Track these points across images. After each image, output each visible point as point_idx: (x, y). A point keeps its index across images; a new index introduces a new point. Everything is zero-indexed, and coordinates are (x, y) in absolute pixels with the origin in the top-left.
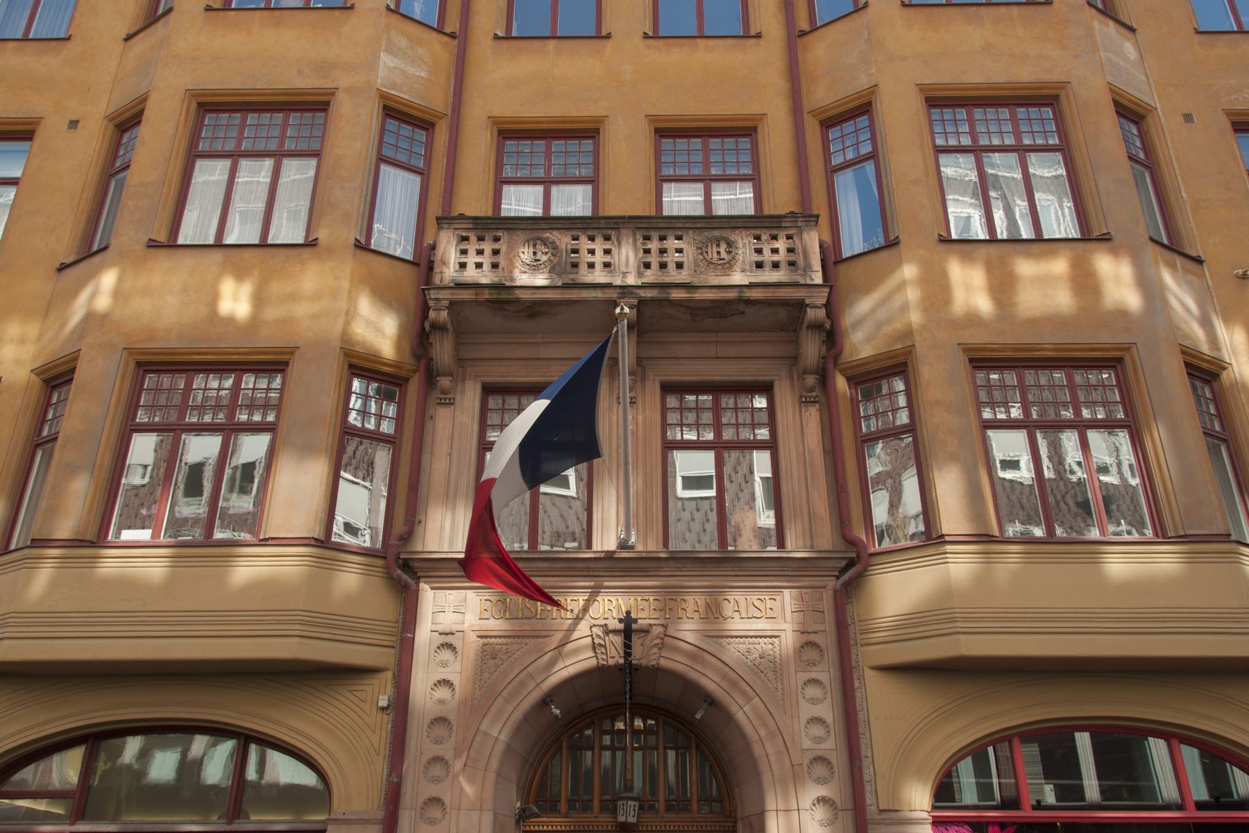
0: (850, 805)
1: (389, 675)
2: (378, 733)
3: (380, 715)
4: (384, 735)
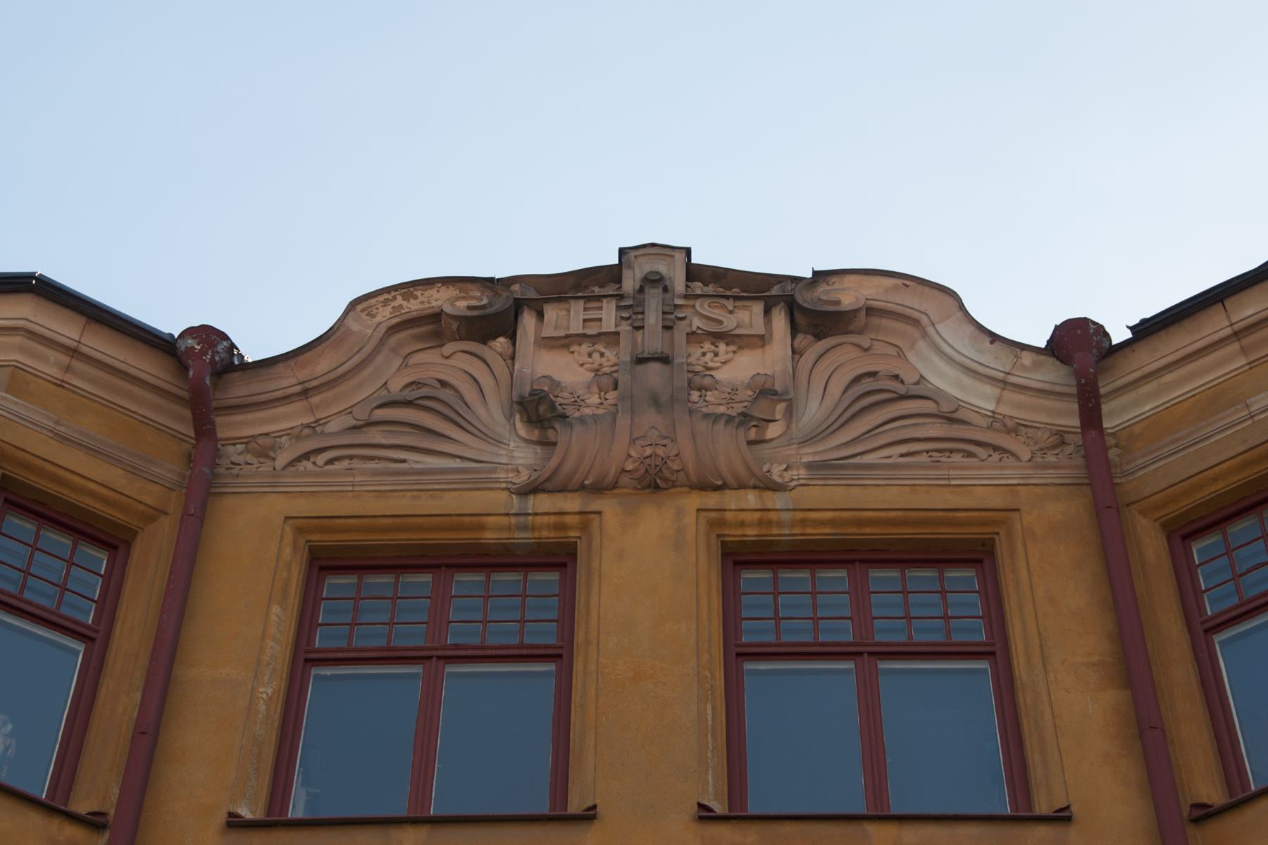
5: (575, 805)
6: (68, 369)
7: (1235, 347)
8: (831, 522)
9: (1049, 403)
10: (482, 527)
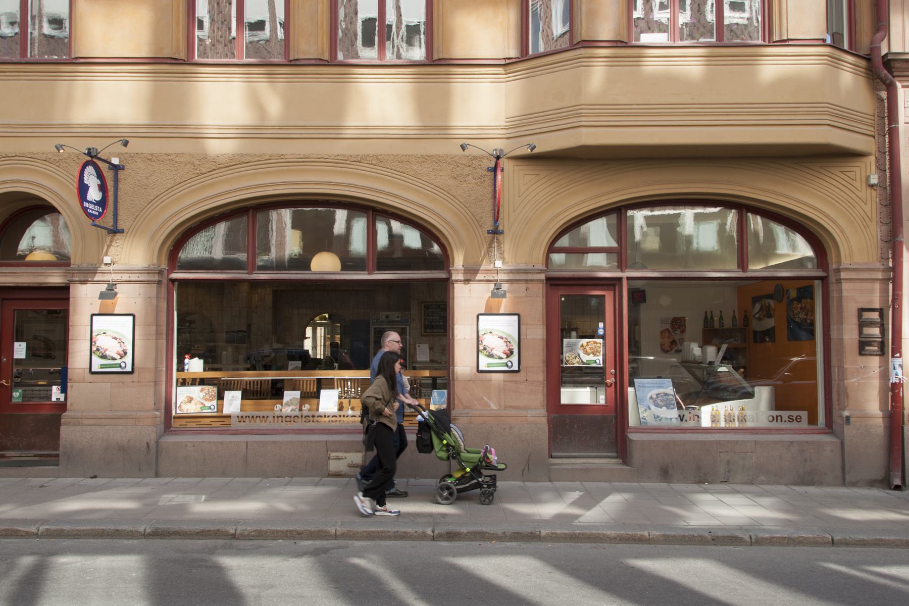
1: (872, 159)
2: (870, 205)
3: (869, 190)
4: (874, 206)
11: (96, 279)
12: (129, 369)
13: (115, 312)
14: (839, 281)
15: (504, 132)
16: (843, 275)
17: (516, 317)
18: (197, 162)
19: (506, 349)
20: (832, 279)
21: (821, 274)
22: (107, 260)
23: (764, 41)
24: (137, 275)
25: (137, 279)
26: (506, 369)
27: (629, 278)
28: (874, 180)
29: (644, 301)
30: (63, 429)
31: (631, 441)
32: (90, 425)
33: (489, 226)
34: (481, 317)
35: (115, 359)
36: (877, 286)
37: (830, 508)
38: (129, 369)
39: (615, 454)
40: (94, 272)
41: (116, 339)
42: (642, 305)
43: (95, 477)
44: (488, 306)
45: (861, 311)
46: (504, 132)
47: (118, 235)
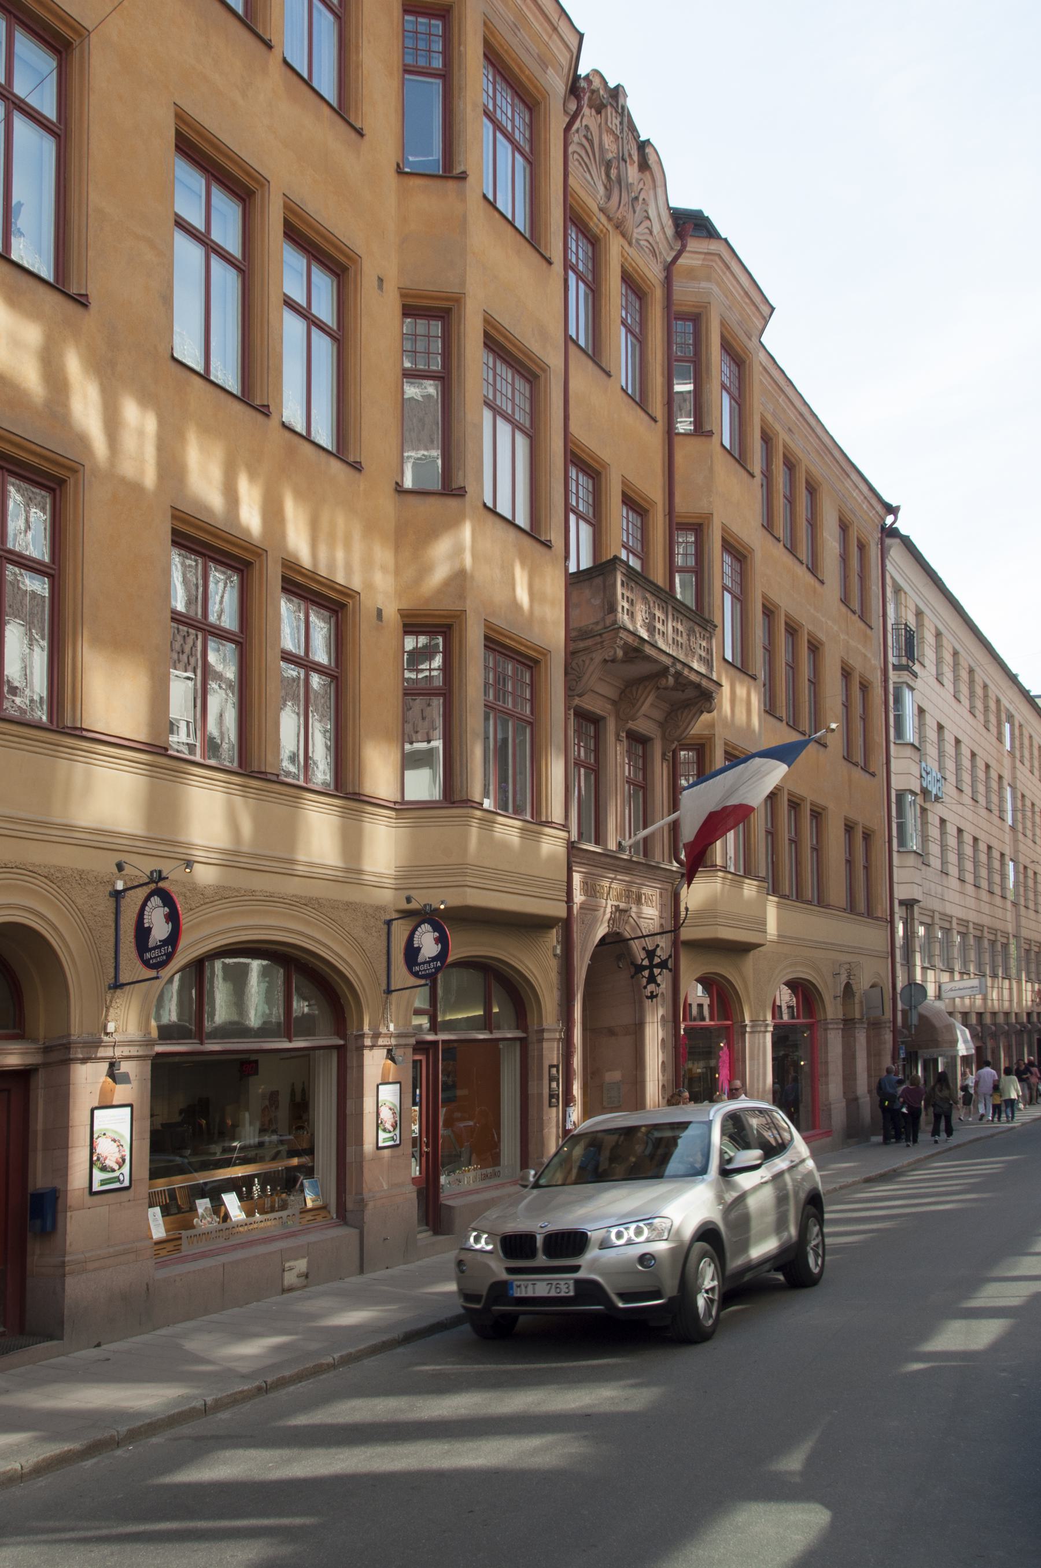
0: (670, 1018)
5: (457, 170)
6: (704, 260)
7: (702, 256)
8: (634, 268)
9: (665, 243)
10: (591, 219)
11: (99, 1055)
12: (126, 1183)
13: (115, 1103)
14: (541, 1041)
15: (393, 881)
16: (546, 1035)
17: (129, 1109)
18: (188, 894)
19: (118, 1156)
20: (533, 1038)
21: (519, 1034)
22: (111, 1027)
23: (532, 818)
24: (137, 1048)
25: (136, 1054)
26: (391, 1143)
27: (443, 1041)
28: (558, 951)
29: (256, 1073)
30: (69, 1281)
31: (450, 1208)
32: (95, 1270)
33: (384, 987)
34: (96, 1112)
35: (113, 1171)
36: (555, 1044)
37: (182, 1396)
38: (126, 1183)
39: (425, 1228)
40: (98, 1044)
41: (114, 1141)
42: (252, 1079)
43: (99, 1345)
44: (103, 1093)
45: (551, 1066)
46: (393, 881)
47: (119, 991)
